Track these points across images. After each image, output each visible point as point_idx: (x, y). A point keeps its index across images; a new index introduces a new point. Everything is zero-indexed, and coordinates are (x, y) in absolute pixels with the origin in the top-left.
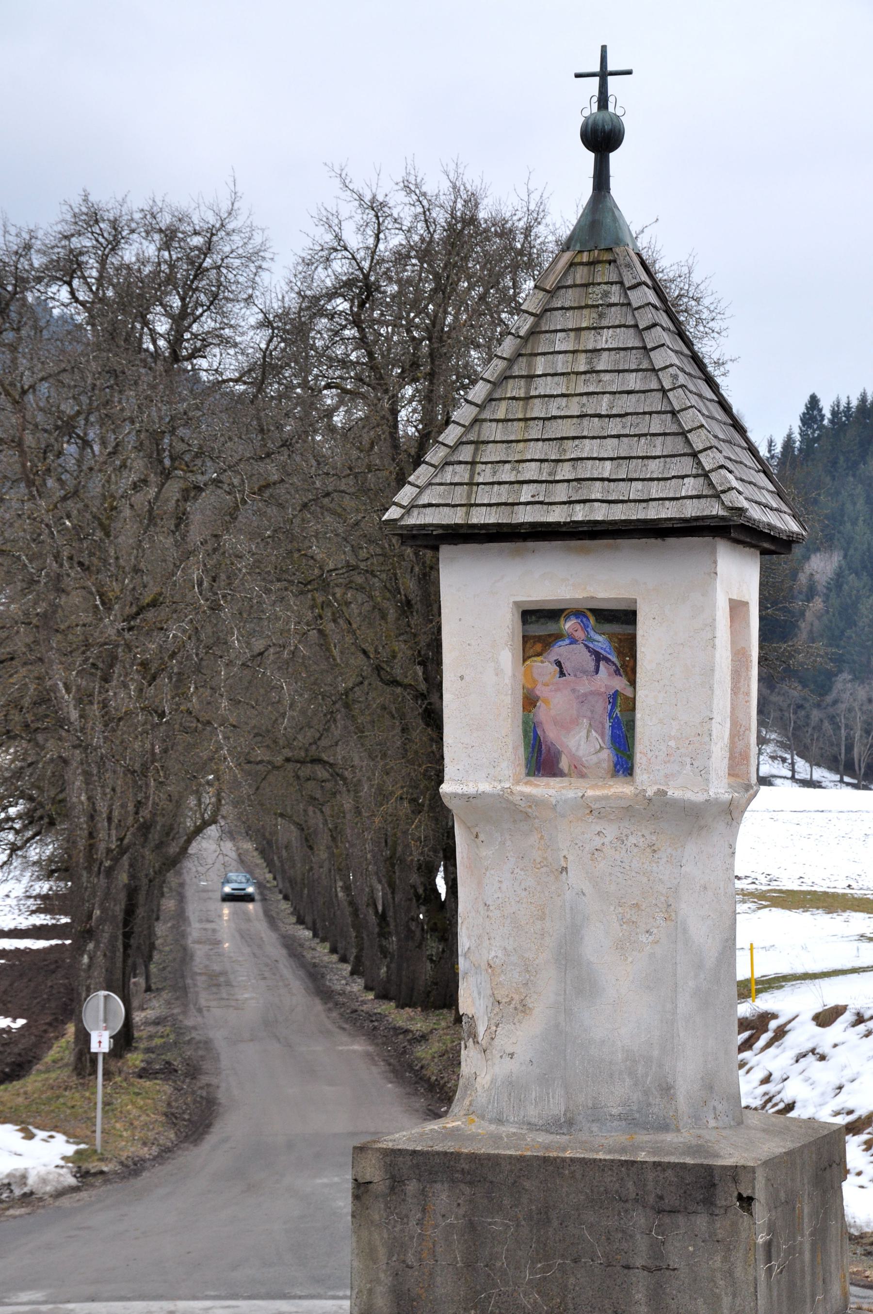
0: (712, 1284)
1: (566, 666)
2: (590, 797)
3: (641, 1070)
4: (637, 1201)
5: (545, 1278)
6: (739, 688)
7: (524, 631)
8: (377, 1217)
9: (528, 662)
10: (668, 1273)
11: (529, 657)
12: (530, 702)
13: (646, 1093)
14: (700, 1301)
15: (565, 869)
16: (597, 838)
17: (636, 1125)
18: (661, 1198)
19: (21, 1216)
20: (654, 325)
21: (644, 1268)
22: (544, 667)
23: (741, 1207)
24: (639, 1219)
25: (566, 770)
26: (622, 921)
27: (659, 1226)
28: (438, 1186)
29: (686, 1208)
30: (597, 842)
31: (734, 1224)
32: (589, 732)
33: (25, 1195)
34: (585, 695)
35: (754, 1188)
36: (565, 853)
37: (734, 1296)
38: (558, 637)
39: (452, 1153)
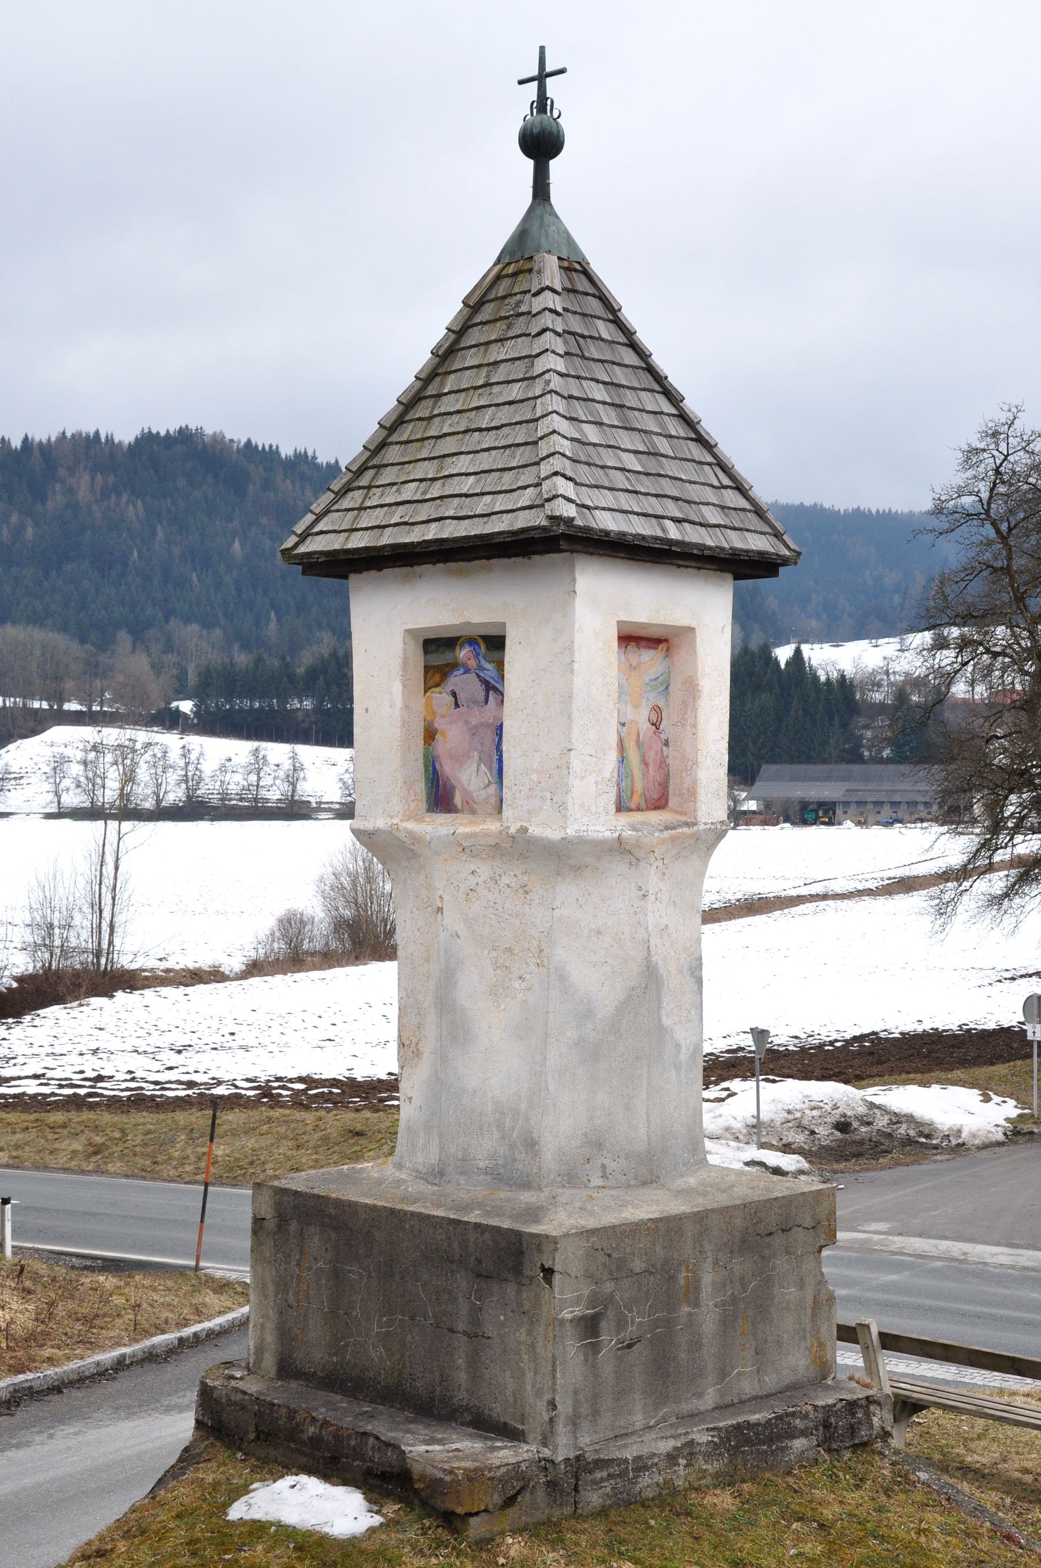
0: (518, 1357)
1: (461, 696)
2: (460, 834)
3: (508, 1123)
4: (460, 1262)
5: (389, 1332)
6: (686, 720)
7: (426, 661)
8: (268, 1254)
9: (428, 694)
10: (484, 1341)
11: (430, 688)
12: (430, 735)
13: (512, 1147)
14: (508, 1373)
15: (440, 910)
16: (471, 877)
17: (501, 1180)
18: (480, 1261)
19: (942, 1161)
20: (544, 331)
21: (465, 1333)
22: (441, 698)
23: (544, 1278)
24: (462, 1281)
25: (460, 807)
26: (496, 966)
27: (477, 1290)
28: (312, 1229)
29: (499, 1275)
30: (472, 881)
31: (537, 1296)
32: (479, 765)
33: (958, 1144)
34: (476, 727)
35: (554, 1260)
36: (441, 892)
37: (536, 1373)
38: (453, 666)
39: (323, 1197)
